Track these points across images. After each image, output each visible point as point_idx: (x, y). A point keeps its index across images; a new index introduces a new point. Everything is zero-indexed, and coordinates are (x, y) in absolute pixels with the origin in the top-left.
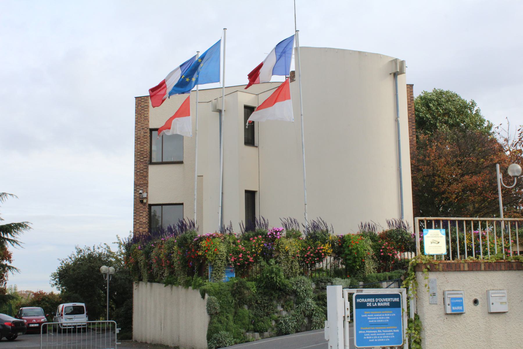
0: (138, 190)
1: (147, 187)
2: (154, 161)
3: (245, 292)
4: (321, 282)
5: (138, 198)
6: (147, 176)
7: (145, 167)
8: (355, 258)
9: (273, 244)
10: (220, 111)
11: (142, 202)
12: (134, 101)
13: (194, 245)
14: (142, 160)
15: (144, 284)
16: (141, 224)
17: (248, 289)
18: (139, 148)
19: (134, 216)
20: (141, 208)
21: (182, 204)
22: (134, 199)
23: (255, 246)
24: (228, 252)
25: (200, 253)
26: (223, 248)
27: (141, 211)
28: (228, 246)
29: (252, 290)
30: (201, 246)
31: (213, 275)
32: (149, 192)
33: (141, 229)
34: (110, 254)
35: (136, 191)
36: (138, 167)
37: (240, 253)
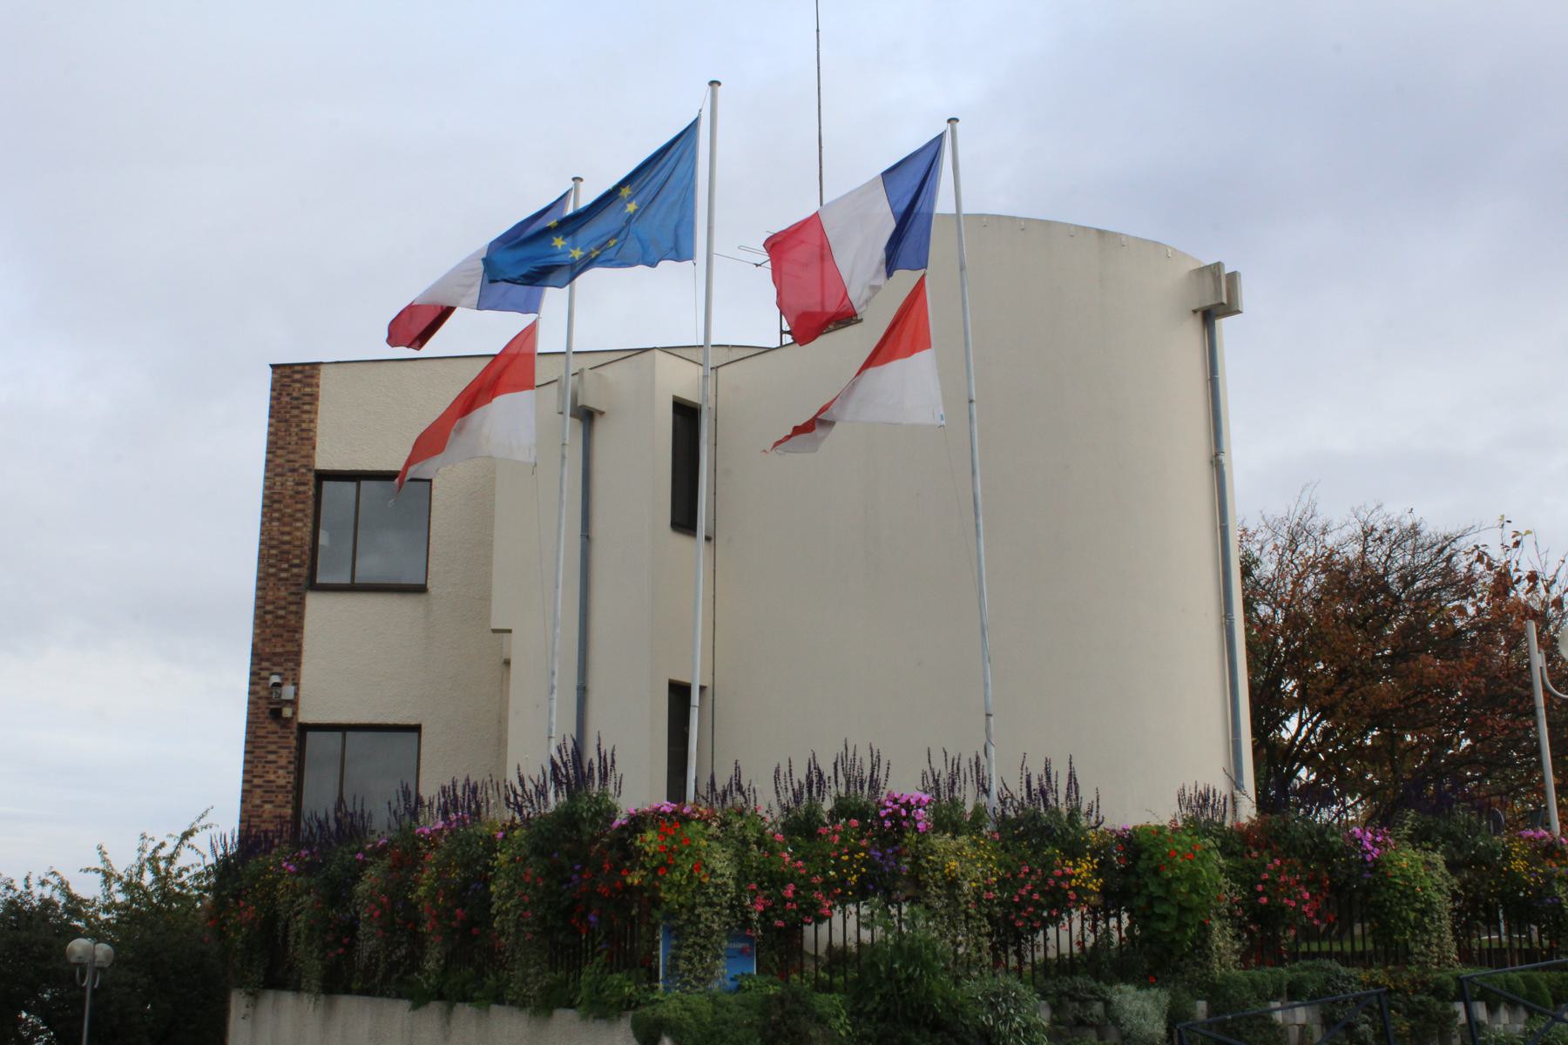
0: (264, 674)
1: (298, 664)
2: (321, 579)
3: (813, 1033)
4: (1072, 999)
5: (262, 703)
6: (298, 629)
7: (291, 599)
8: (1183, 909)
9: (898, 854)
10: (587, 417)
11: (276, 714)
12: (267, 377)
13: (610, 846)
14: (283, 575)
15: (307, 1001)
16: (269, 790)
17: (821, 1020)
18: (275, 533)
19: (246, 762)
20: (274, 738)
21: (417, 729)
22: (250, 703)
23: (837, 859)
24: (742, 878)
25: (634, 879)
26: (721, 862)
27: (272, 747)
28: (740, 857)
29: (836, 1024)
30: (640, 851)
31: (683, 965)
32: (303, 681)
33: (268, 807)
34: (75, 905)
35: (256, 677)
36: (269, 598)
37: (783, 884)
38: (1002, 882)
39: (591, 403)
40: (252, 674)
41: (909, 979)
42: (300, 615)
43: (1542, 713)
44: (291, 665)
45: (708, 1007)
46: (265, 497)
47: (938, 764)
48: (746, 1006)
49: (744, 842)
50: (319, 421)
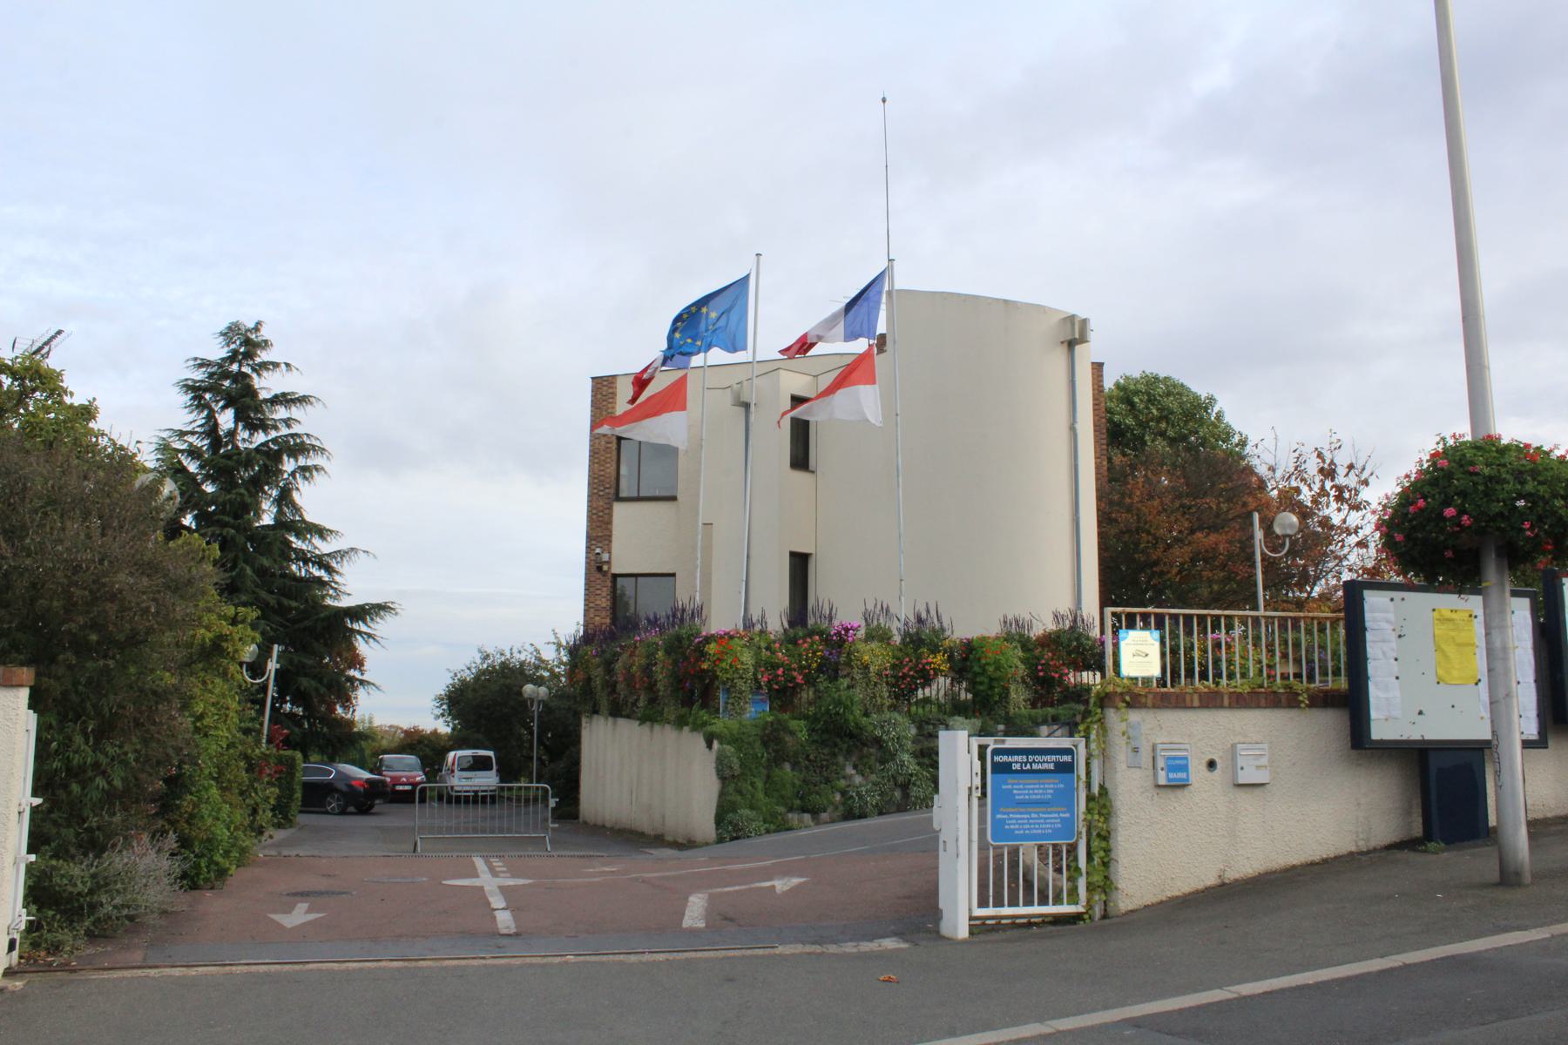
2: (623, 494)
8: (991, 679)
11: (599, 569)
12: (589, 384)
16: (597, 609)
17: (792, 733)
21: (673, 575)
24: (757, 665)
25: (705, 666)
26: (747, 658)
35: (589, 549)
38: (894, 667)
41: (837, 713)
42: (610, 515)
43: (1259, 565)
47: (870, 607)
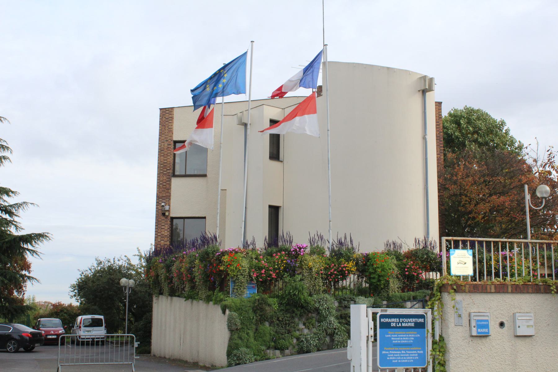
0: (160, 202)
1: (170, 199)
3: (267, 309)
4: (344, 300)
6: (169, 189)
7: (167, 180)
8: (379, 276)
9: (296, 261)
10: (245, 125)
11: (164, 214)
12: (158, 112)
16: (163, 237)
17: (269, 305)
20: (163, 221)
21: (205, 218)
23: (278, 262)
24: (250, 268)
27: (163, 224)
28: (251, 262)
29: (274, 306)
31: (235, 291)
32: (171, 205)
33: (162, 242)
35: (158, 203)
39: (245, 121)
40: (157, 202)
41: (295, 295)
42: (170, 185)
43: (528, 214)
44: (168, 200)
45: (239, 301)
46: (159, 149)
48: (250, 302)
49: (252, 258)
50: (174, 125)
